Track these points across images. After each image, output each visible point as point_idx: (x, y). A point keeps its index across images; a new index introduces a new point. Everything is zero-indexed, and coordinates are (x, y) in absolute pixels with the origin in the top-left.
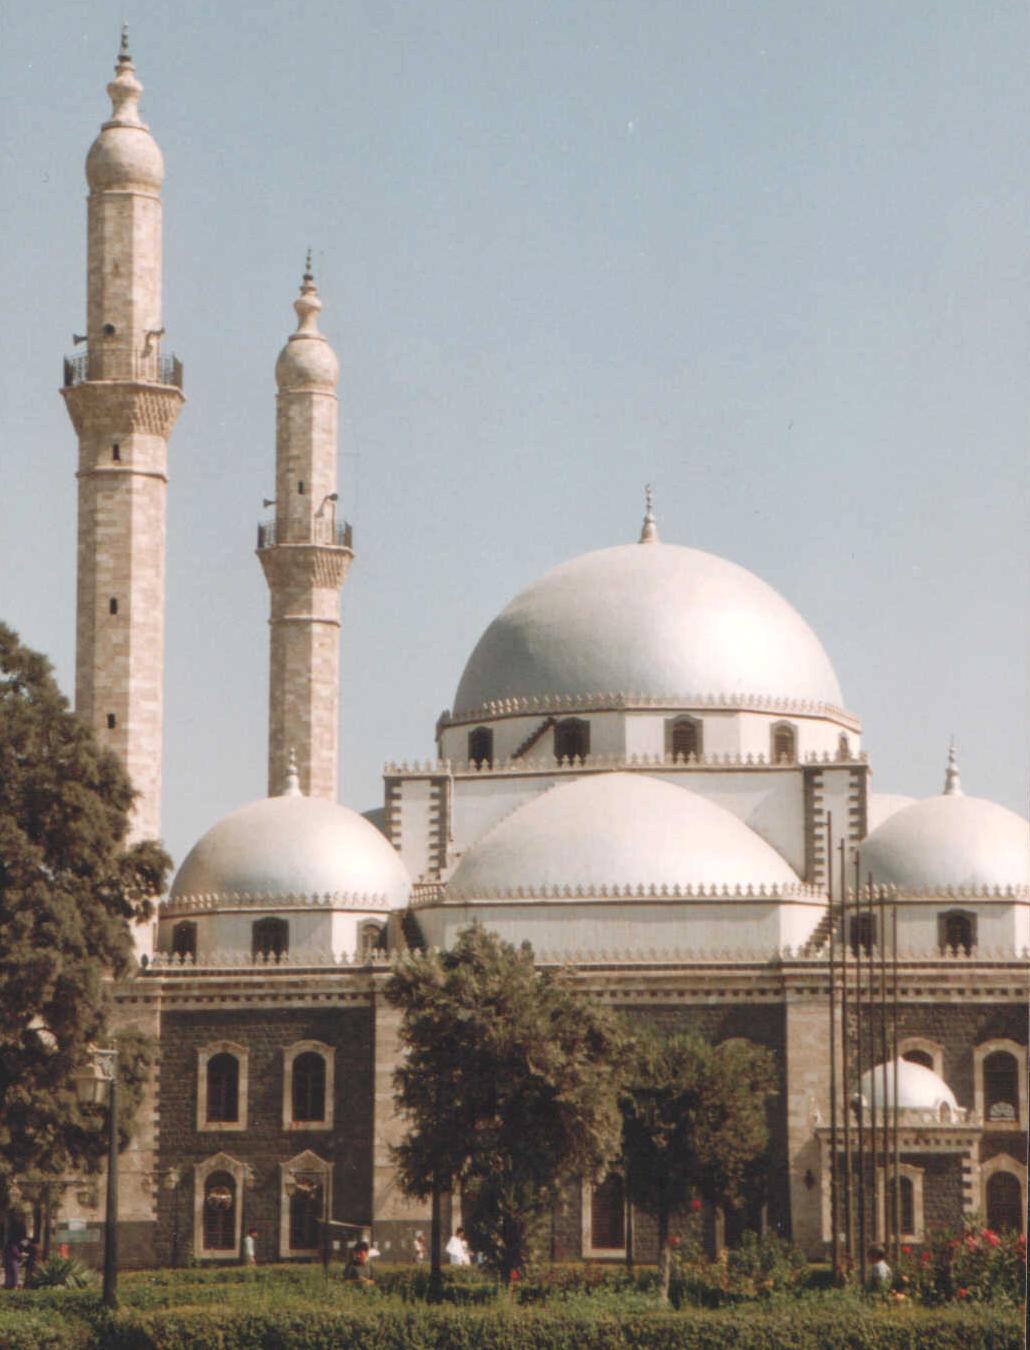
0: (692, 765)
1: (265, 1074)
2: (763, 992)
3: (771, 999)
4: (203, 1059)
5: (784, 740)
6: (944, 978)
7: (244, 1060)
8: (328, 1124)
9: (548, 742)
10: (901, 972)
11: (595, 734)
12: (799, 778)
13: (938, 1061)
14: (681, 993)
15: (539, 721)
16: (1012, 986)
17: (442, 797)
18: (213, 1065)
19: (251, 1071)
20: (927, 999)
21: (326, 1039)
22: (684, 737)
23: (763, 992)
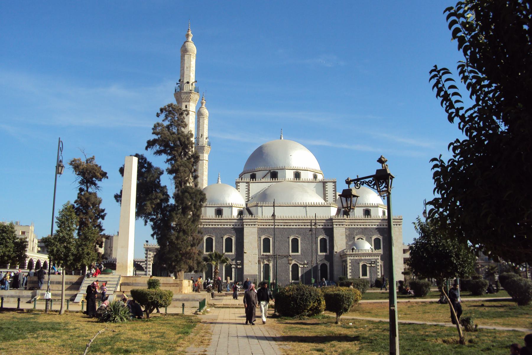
0: (276, 181)
1: (219, 243)
2: (328, 225)
3: (330, 227)
4: (205, 238)
5: (315, 177)
6: (255, 222)
7: (214, 238)
8: (299, 253)
9: (269, 175)
10: (317, 221)
11: (279, 175)
12: (322, 184)
13: (364, 239)
14: (269, 225)
15: (268, 171)
16: (385, 224)
17: (249, 186)
18: (207, 240)
19: (216, 241)
20: (362, 226)
21: (300, 234)
22: (297, 175)
23: (328, 225)
